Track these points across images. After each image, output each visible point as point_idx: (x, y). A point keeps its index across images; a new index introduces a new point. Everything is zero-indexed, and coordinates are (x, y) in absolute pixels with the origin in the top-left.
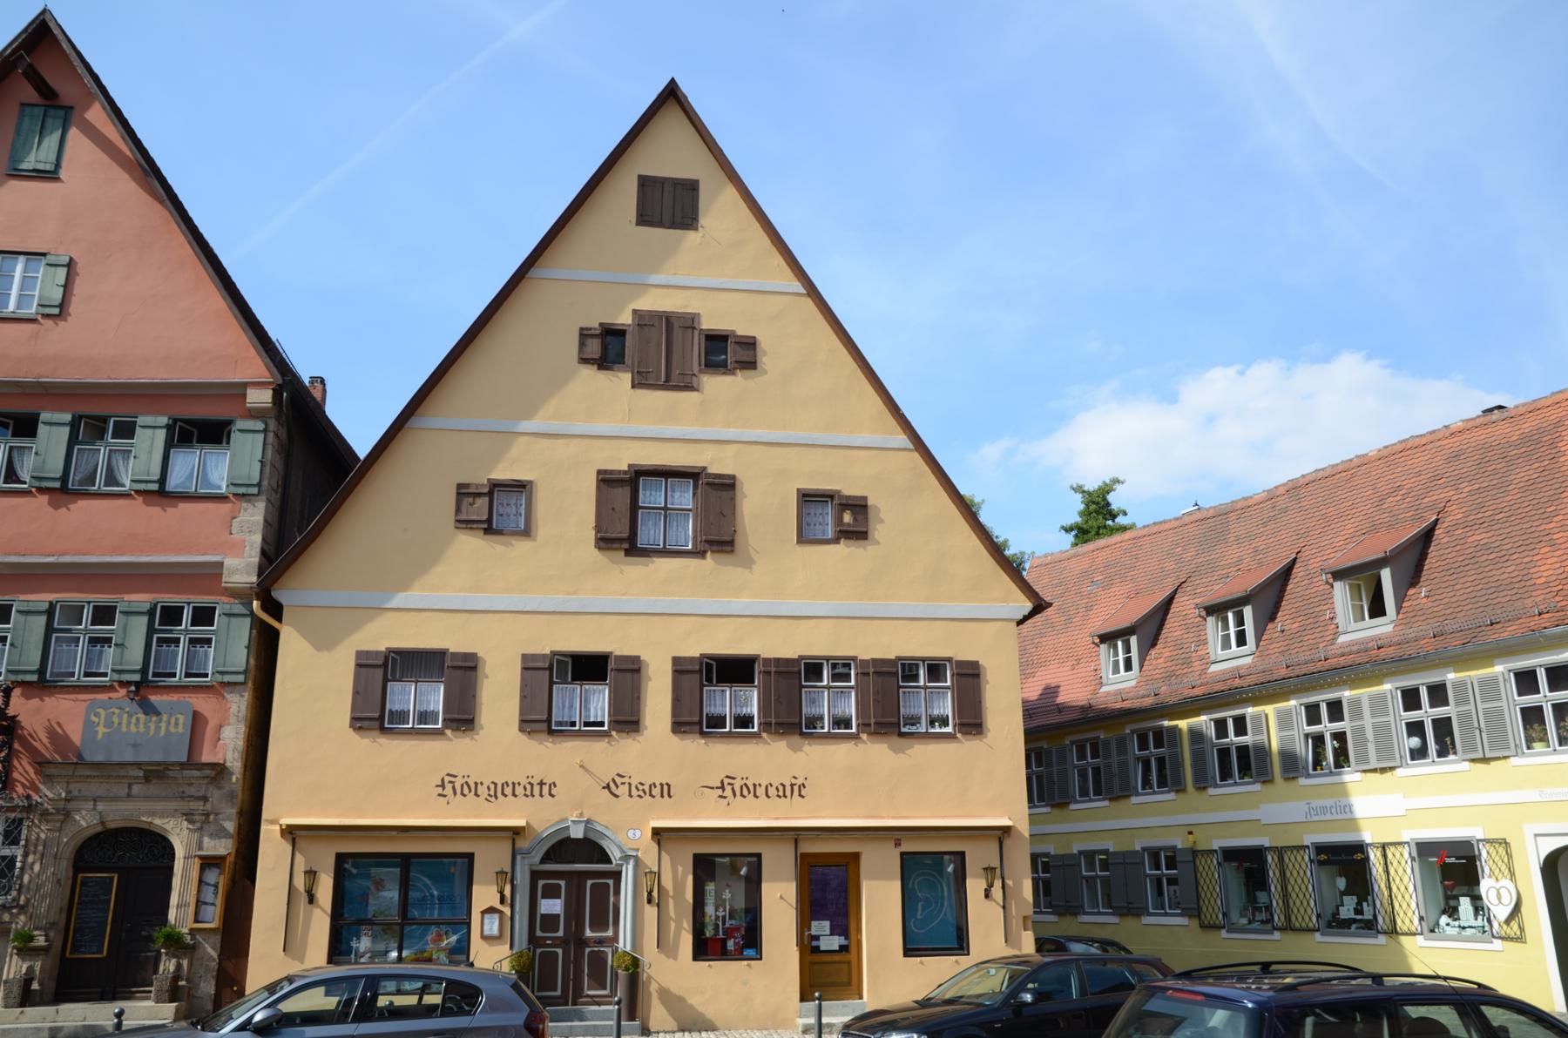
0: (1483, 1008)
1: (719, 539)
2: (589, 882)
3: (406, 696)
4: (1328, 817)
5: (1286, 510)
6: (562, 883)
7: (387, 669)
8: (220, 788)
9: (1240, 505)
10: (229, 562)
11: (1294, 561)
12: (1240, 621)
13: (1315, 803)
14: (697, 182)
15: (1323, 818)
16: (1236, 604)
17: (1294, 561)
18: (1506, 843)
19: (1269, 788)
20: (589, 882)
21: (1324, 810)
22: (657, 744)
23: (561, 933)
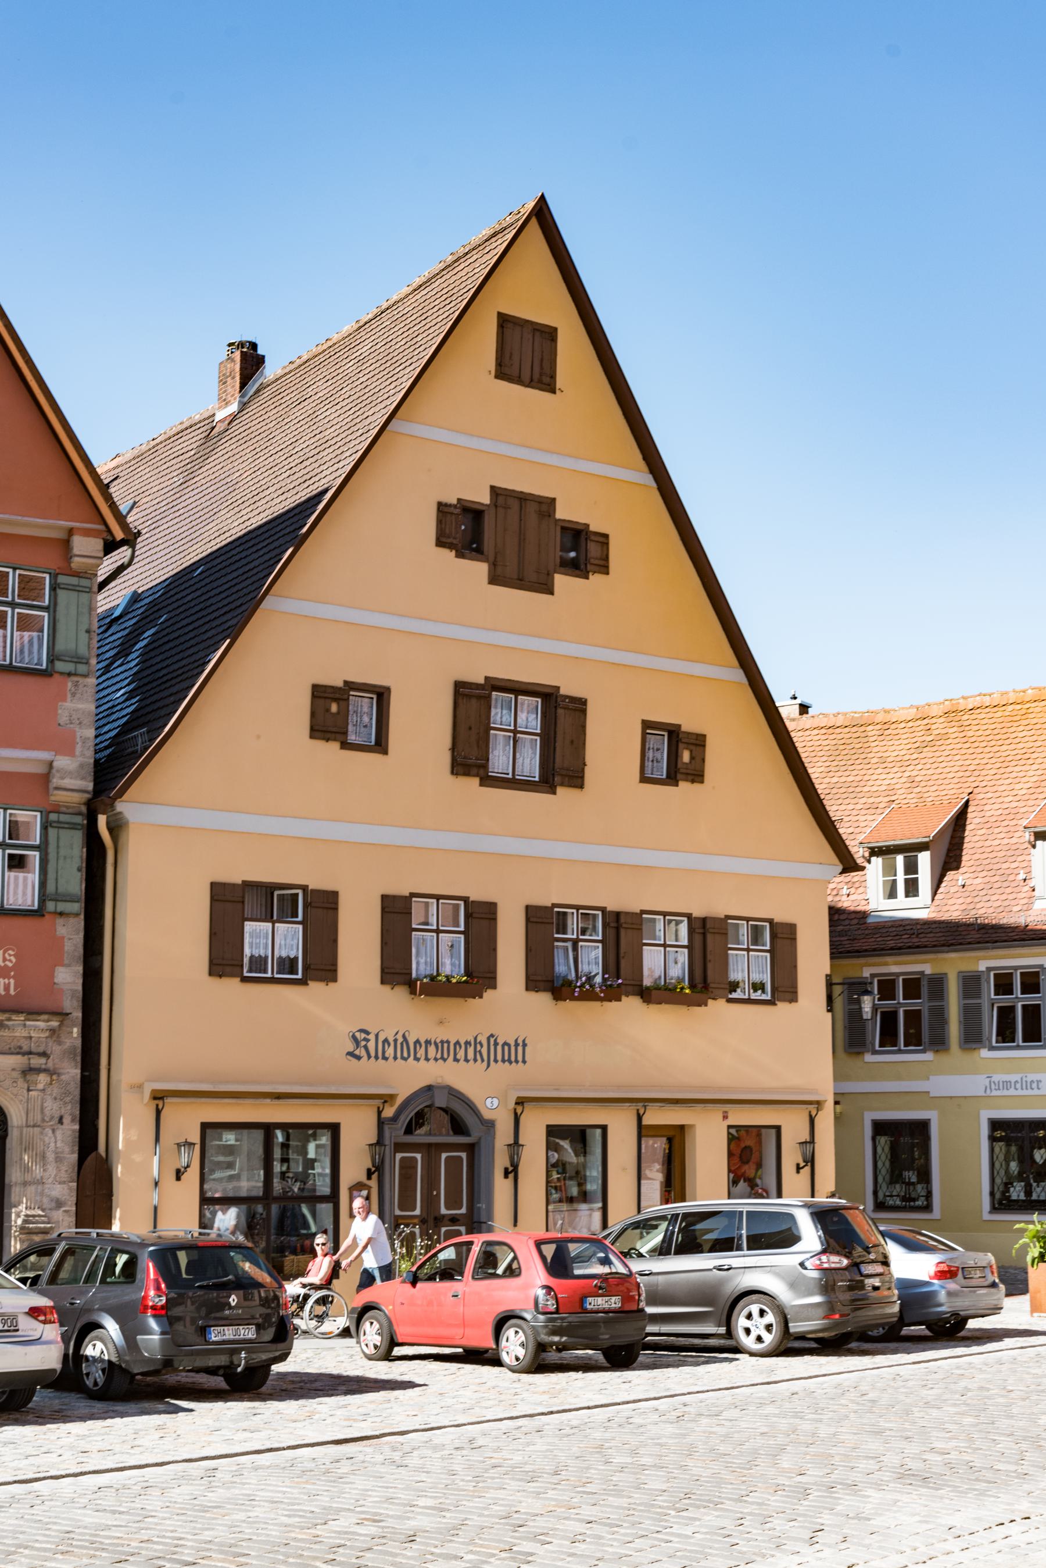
0: (227, 1387)
1: (561, 767)
2: (444, 1156)
3: (258, 937)
4: (1012, 1092)
5: (945, 736)
6: (418, 1156)
7: (233, 905)
8: (60, 1043)
9: (880, 718)
10: (62, 762)
11: (967, 804)
12: (911, 867)
13: (997, 1078)
14: (556, 329)
15: (1005, 1093)
16: (910, 850)
17: (967, 804)
18: (520, 1102)
19: (943, 1059)
20: (444, 1156)
21: (1007, 1084)
22: (511, 1003)
23: (417, 1212)
